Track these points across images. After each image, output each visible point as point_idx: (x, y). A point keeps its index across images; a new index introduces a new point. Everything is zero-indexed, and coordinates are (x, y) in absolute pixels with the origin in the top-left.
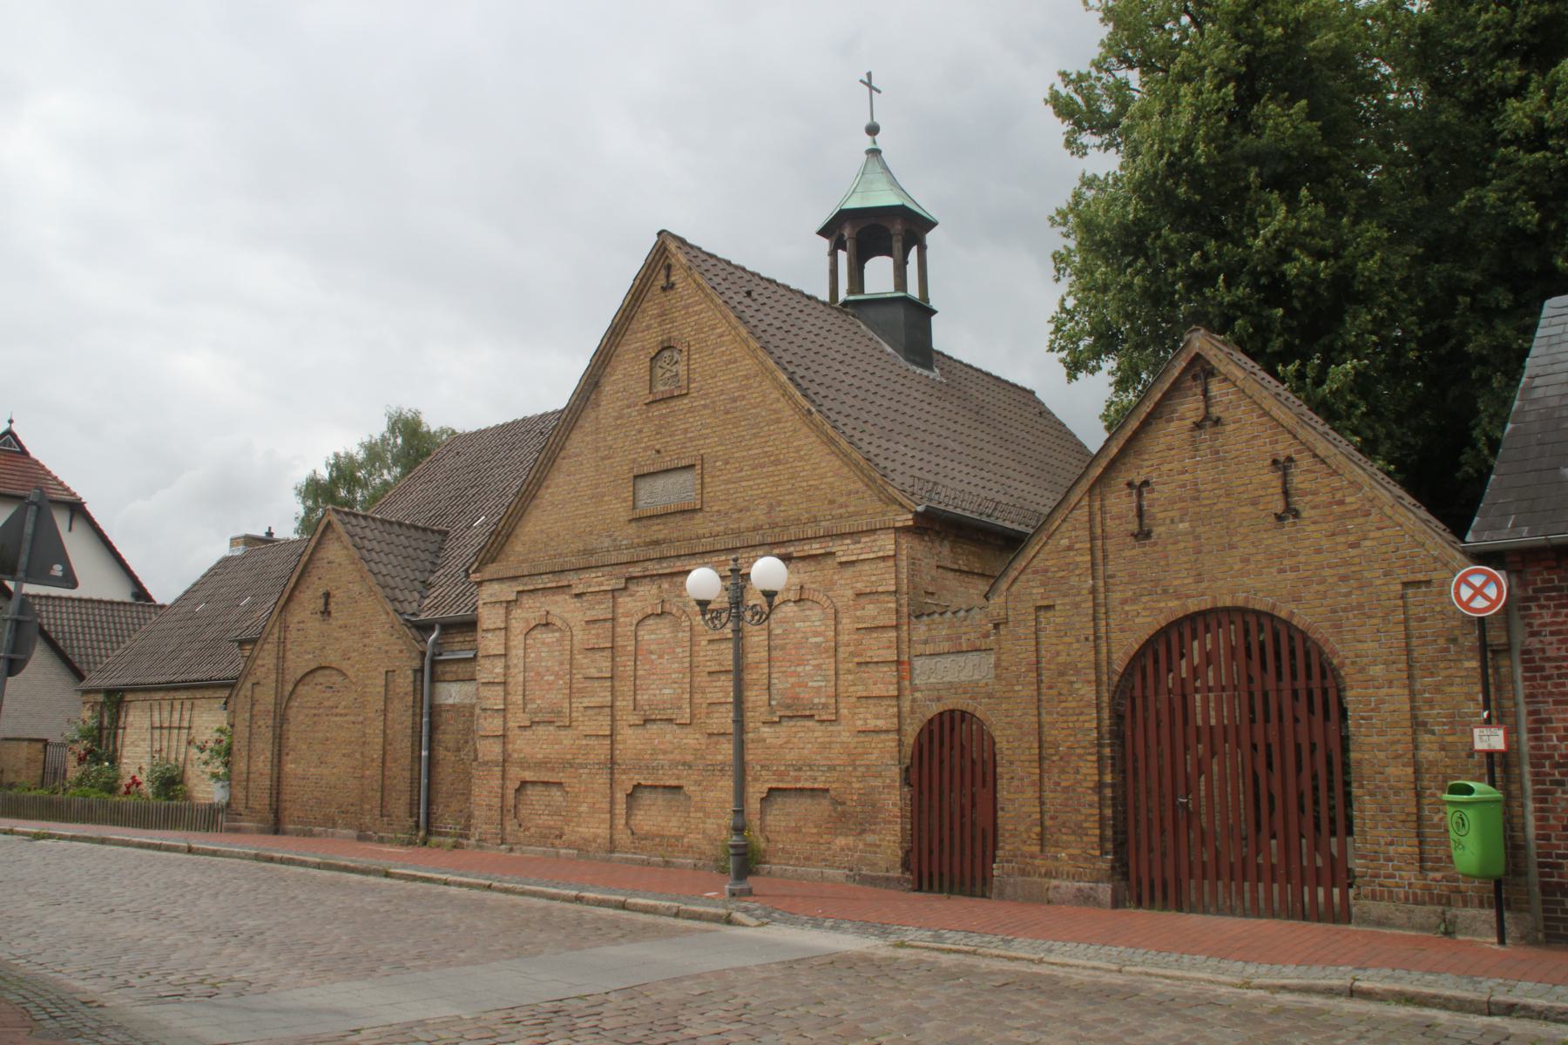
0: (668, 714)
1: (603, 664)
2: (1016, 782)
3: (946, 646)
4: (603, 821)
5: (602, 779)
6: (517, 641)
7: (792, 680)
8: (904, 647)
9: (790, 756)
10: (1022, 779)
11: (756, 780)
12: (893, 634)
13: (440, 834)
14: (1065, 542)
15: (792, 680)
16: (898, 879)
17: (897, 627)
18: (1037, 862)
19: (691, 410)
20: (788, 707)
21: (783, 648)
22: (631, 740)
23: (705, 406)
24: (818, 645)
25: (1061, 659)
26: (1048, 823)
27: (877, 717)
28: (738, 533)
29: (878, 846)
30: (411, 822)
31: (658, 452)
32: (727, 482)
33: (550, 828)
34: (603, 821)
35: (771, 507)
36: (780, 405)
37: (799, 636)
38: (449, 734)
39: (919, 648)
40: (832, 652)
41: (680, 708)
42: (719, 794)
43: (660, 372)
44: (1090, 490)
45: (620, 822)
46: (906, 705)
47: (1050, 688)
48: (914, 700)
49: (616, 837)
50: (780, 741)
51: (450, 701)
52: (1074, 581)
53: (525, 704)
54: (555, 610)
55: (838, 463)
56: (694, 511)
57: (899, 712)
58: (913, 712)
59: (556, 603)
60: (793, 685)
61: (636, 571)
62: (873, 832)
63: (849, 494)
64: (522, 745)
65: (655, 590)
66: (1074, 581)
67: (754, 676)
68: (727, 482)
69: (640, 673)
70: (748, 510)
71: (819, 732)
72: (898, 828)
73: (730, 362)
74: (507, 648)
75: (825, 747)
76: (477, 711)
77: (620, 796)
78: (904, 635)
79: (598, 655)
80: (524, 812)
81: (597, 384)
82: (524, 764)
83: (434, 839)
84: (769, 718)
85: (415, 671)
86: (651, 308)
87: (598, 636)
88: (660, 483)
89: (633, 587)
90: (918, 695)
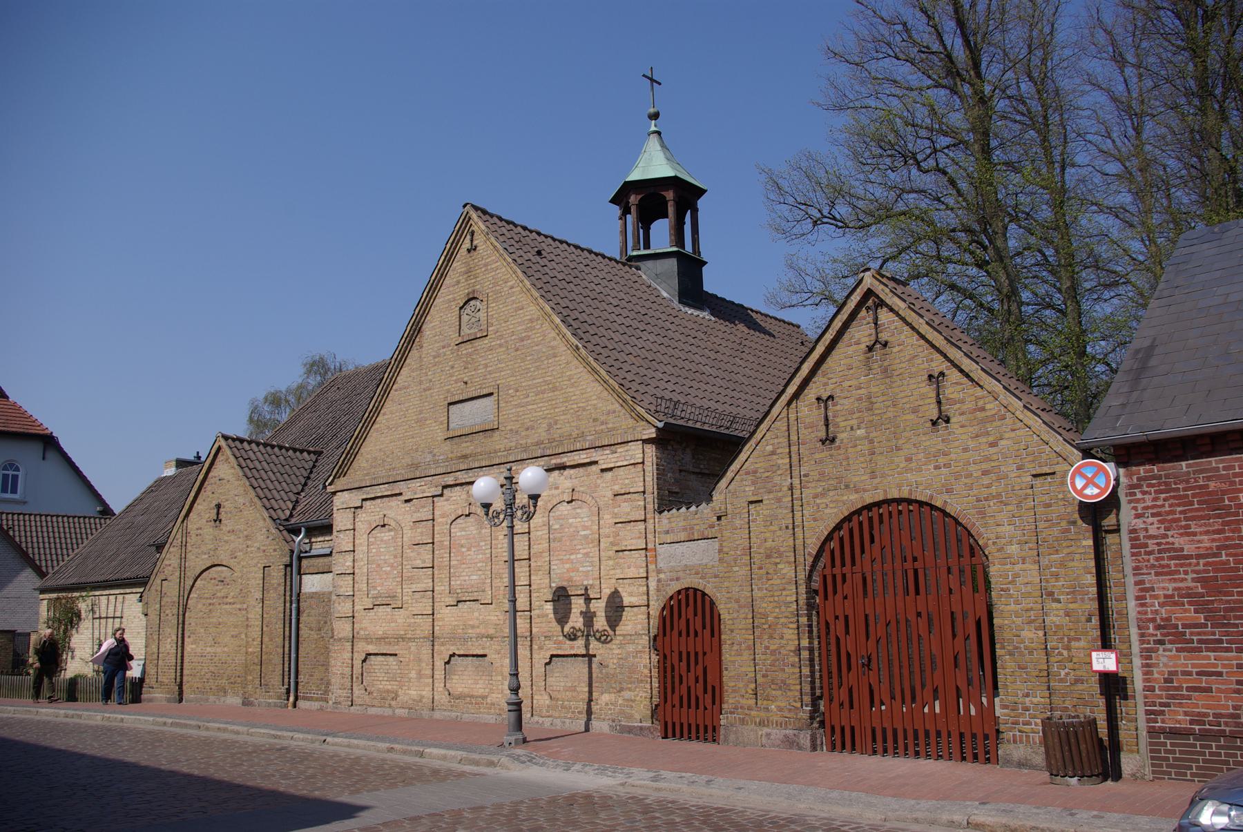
5: (426, 651)
7: (567, 566)
8: (650, 536)
11: (541, 648)
14: (769, 448)
15: (567, 566)
16: (649, 728)
18: (753, 713)
22: (448, 617)
23: (501, 346)
24: (586, 537)
26: (760, 680)
28: (526, 448)
29: (633, 701)
44: (789, 403)
45: (439, 686)
46: (653, 584)
48: (659, 581)
62: (630, 689)
76: (334, 597)
77: (439, 664)
82: (368, 640)
85: (286, 566)
90: (662, 576)
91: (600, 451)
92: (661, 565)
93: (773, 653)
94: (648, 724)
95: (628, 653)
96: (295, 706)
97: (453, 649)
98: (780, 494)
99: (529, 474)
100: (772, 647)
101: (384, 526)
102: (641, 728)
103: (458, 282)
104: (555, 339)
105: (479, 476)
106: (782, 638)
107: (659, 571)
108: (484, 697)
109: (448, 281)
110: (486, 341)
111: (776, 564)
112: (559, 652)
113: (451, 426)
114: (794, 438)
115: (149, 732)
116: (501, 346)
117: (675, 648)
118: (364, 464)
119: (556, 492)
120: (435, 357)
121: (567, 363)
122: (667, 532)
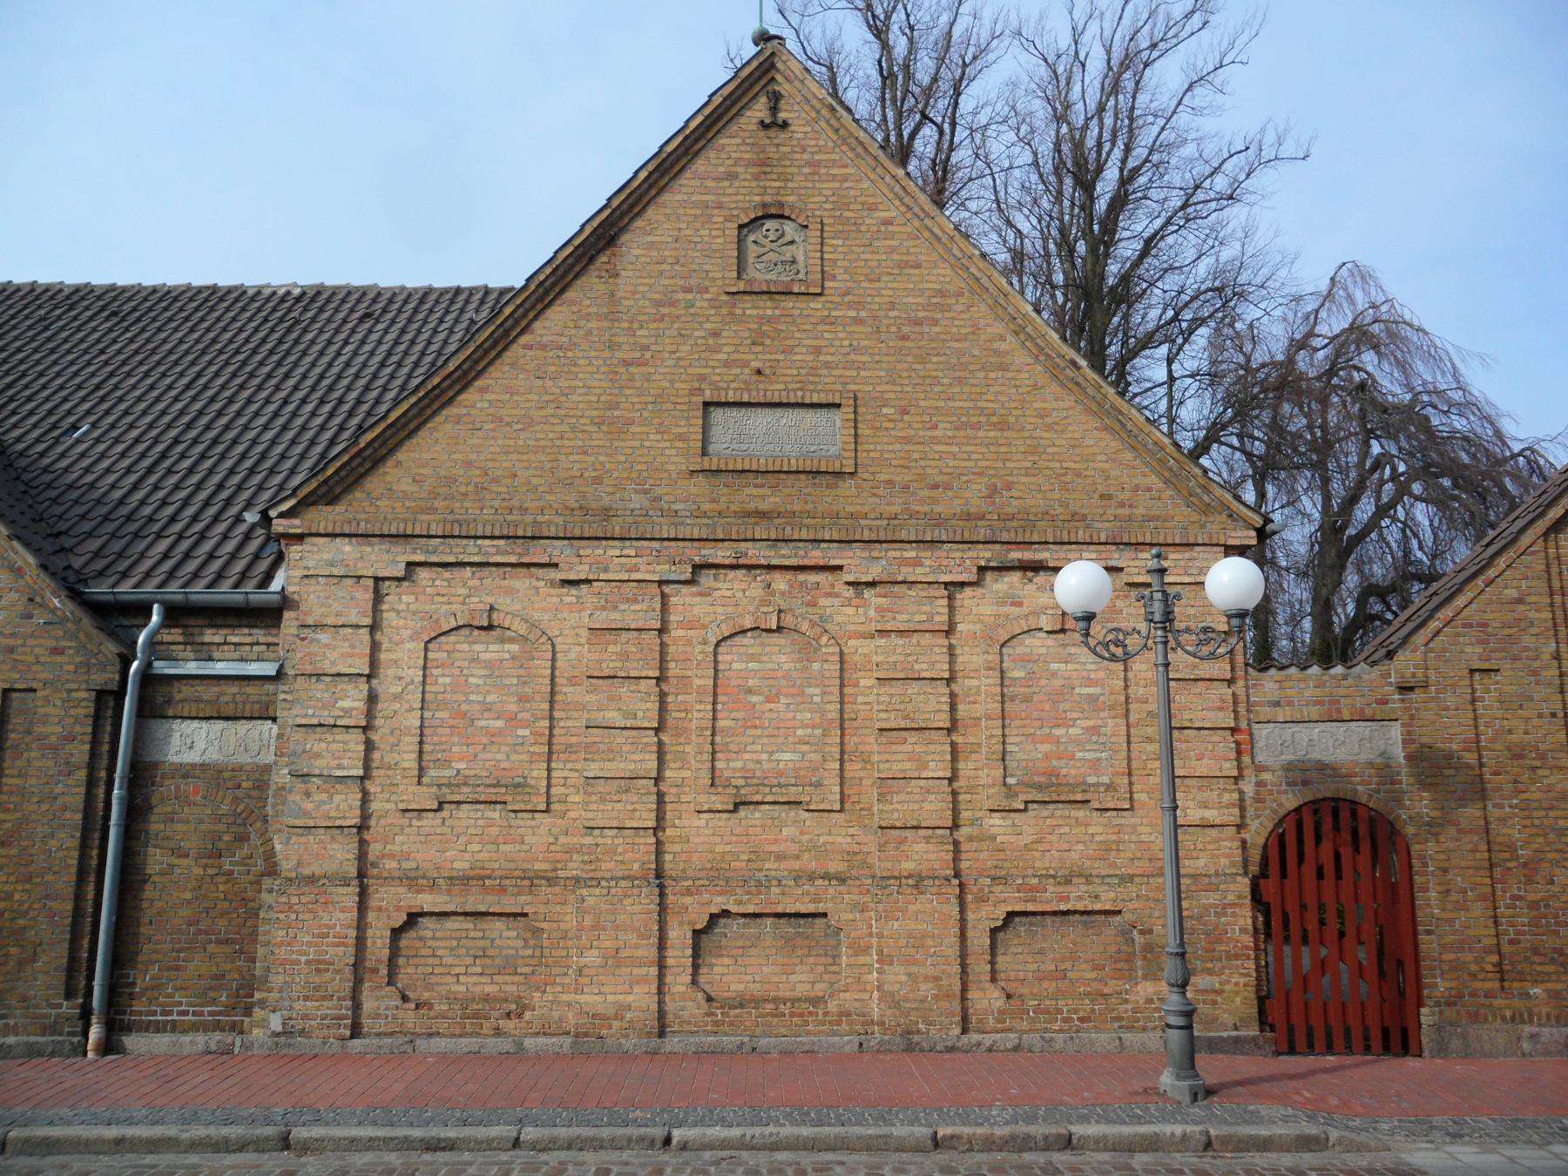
0: (793, 793)
1: (931, 705)
2: (1454, 896)
3: (1314, 711)
4: (643, 980)
5: (641, 905)
6: (403, 657)
7: (1046, 748)
8: (1242, 710)
9: (1045, 862)
10: (1464, 891)
11: (982, 899)
12: (1226, 692)
13: (146, 1027)
14: (1511, 593)
15: (1046, 748)
16: (1254, 1039)
17: (1230, 682)
18: (1498, 1002)
19: (829, 321)
20: (1040, 787)
21: (1027, 700)
22: (699, 834)
23: (858, 321)
24: (1092, 699)
25: (1514, 738)
26: (1506, 948)
27: (1204, 805)
28: (939, 522)
29: (1219, 992)
30: (69, 1008)
31: (759, 372)
32: (906, 440)
33: (486, 998)
34: (643, 980)
35: (993, 491)
36: (1004, 346)
37: (1058, 683)
38: (178, 830)
39: (1265, 712)
40: (1121, 711)
41: (818, 785)
42: (911, 925)
43: (752, 248)
44: (1546, 535)
45: (679, 982)
46: (1248, 787)
47: (1497, 773)
48: (1259, 784)
49: (670, 1007)
50: (1026, 839)
51: (191, 757)
52: (1527, 641)
53: (421, 770)
54: (502, 602)
55: (1114, 444)
56: (838, 474)
57: (1242, 800)
58: (1258, 799)
59: (511, 591)
60: (1047, 756)
61: (722, 554)
62: (1210, 972)
63: (1136, 489)
64: (403, 844)
65: (756, 590)
66: (1527, 641)
67: (980, 737)
68: (906, 440)
69: (721, 724)
70: (948, 487)
71: (1098, 827)
72: (1251, 965)
73: (907, 264)
74: (374, 664)
75: (1107, 848)
76: (281, 777)
77: (679, 935)
78: (1241, 692)
79: (624, 690)
80: (407, 973)
81: (612, 241)
82: (412, 880)
83: (132, 1041)
84: (1004, 804)
85: (101, 694)
86: (733, 145)
87: (625, 656)
88: (762, 420)
89: (707, 578)
90: (1267, 776)
91: (1129, 553)
92: (1260, 758)
93: (1533, 905)
94: (1254, 1031)
95: (1206, 907)
96: (109, 1046)
97: (718, 903)
98: (1536, 664)
99: (1225, 577)
100: (1531, 897)
101: (490, 627)
102: (1236, 1040)
103: (732, 176)
104: (1003, 338)
105: (1069, 561)
106: (1552, 882)
107: (1260, 769)
108: (816, 1001)
109: (700, 166)
110: (816, 304)
111: (1534, 769)
112: (1030, 907)
113: (711, 448)
114: (1556, 584)
115: (859, 1138)
116: (858, 321)
117: (1310, 899)
118: (406, 486)
119: (1016, 610)
120: (658, 304)
121: (1035, 386)
122: (1277, 704)
